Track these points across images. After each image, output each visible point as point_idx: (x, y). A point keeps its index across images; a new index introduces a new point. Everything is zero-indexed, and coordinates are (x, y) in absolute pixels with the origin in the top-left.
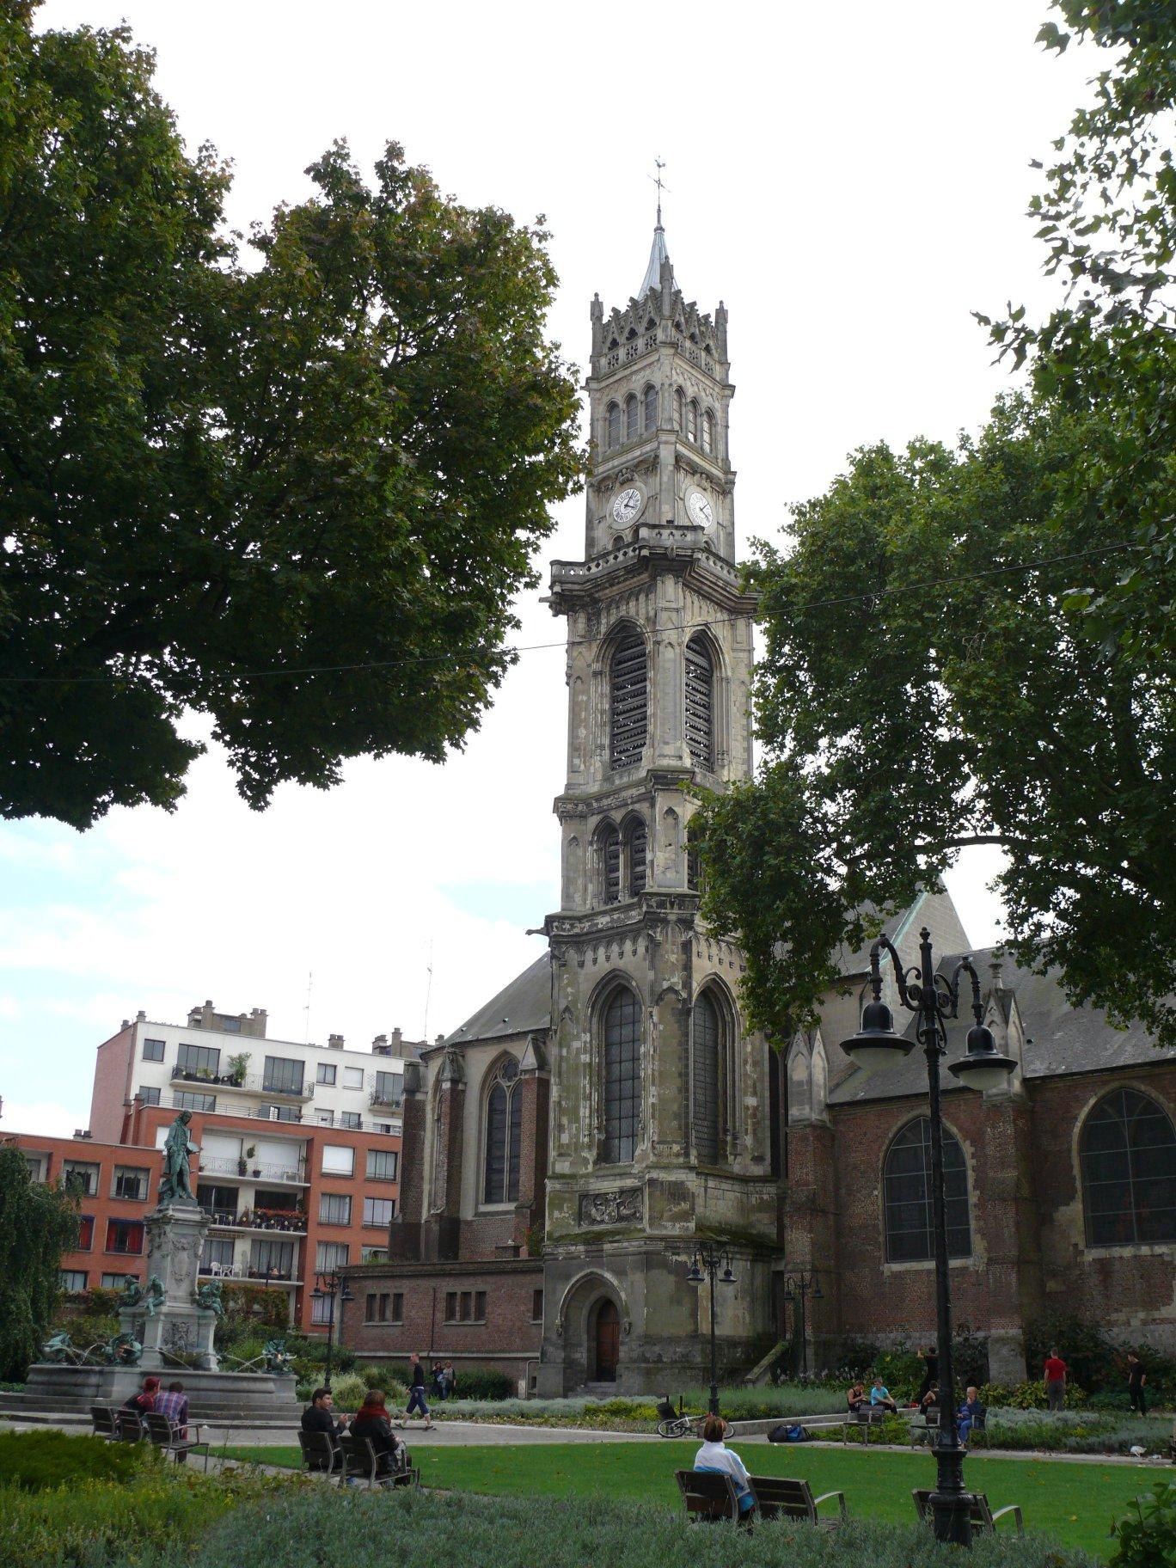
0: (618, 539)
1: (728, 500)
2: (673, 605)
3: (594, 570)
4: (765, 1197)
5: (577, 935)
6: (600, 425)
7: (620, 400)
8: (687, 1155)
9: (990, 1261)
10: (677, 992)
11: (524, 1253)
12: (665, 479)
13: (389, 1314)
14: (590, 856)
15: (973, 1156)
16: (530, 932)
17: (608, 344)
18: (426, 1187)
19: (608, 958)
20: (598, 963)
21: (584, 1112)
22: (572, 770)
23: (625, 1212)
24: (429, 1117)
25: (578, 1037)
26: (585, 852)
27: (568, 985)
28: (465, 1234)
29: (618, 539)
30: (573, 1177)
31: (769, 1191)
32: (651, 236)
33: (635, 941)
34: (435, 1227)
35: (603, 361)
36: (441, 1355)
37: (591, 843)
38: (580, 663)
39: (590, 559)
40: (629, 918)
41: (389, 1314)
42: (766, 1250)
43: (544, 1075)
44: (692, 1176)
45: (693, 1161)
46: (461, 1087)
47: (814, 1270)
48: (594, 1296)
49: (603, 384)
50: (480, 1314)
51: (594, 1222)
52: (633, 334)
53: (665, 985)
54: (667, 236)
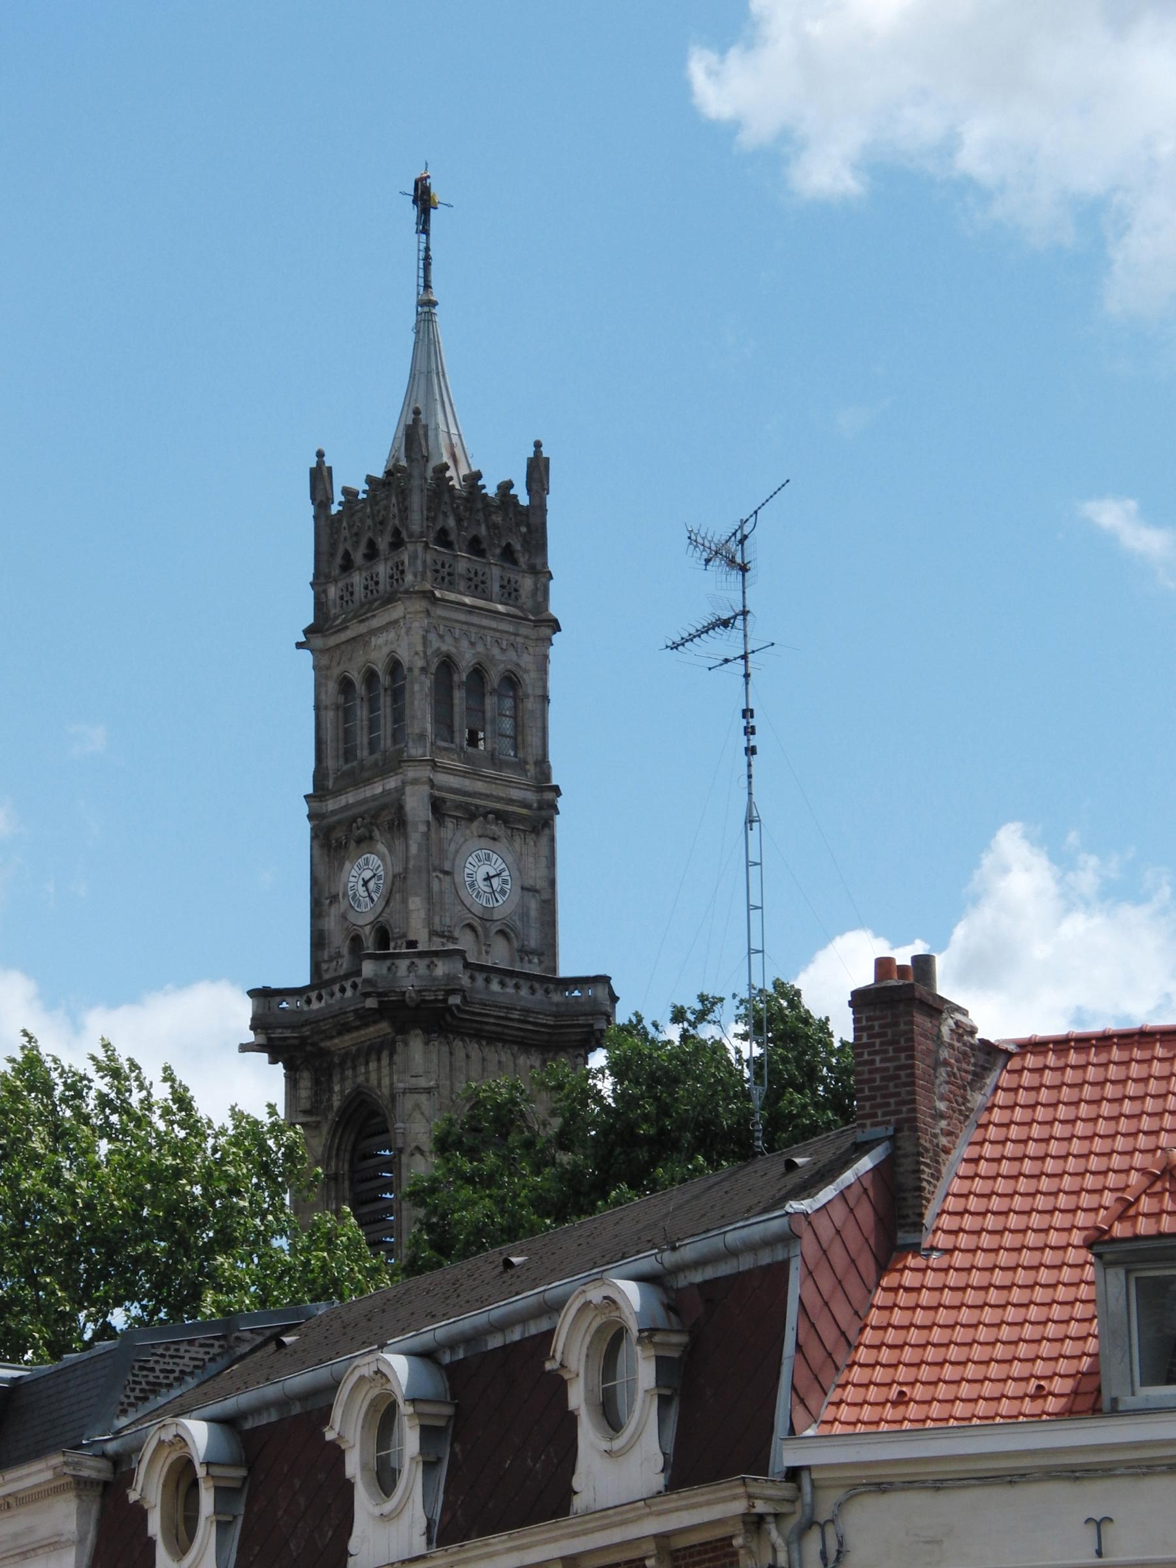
1: (544, 840)
2: (423, 1083)
6: (330, 715)
7: (356, 677)
12: (414, 849)
17: (339, 560)
29: (356, 941)
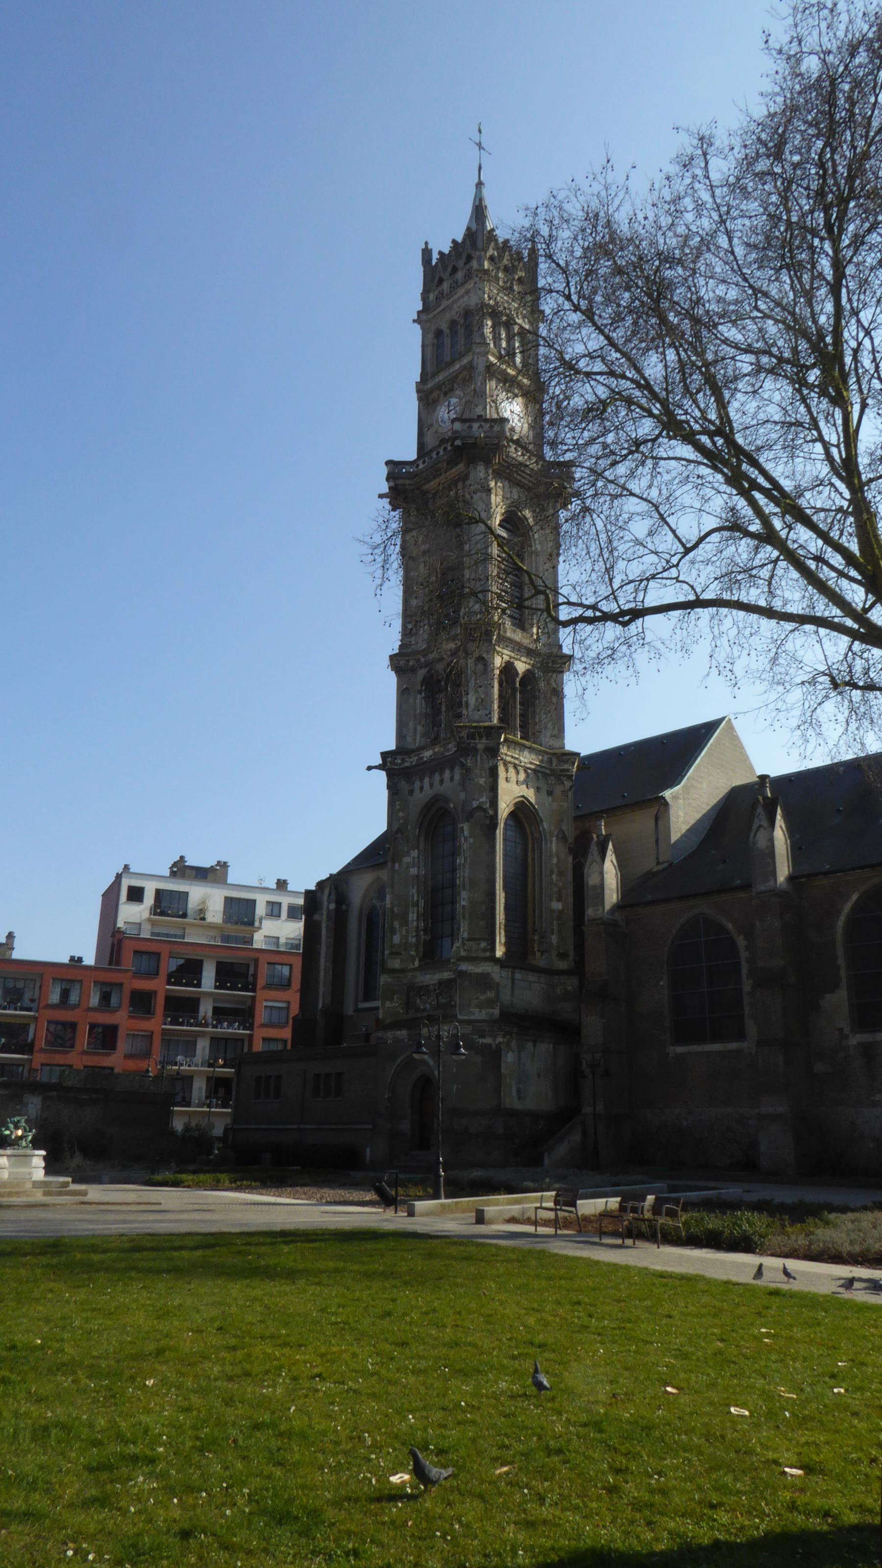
3: (421, 466)
4: (569, 988)
5: (407, 768)
6: (429, 350)
7: (444, 326)
10: (485, 810)
14: (419, 702)
15: (747, 948)
16: (369, 768)
19: (431, 785)
21: (412, 916)
23: (442, 1001)
25: (407, 854)
26: (415, 699)
27: (400, 810)
30: (402, 971)
31: (572, 983)
32: (473, 190)
33: (452, 770)
36: (308, 1126)
37: (420, 692)
40: (448, 750)
42: (566, 1032)
44: (497, 969)
46: (344, 907)
49: (431, 315)
52: (455, 270)
53: (475, 804)
54: (485, 192)
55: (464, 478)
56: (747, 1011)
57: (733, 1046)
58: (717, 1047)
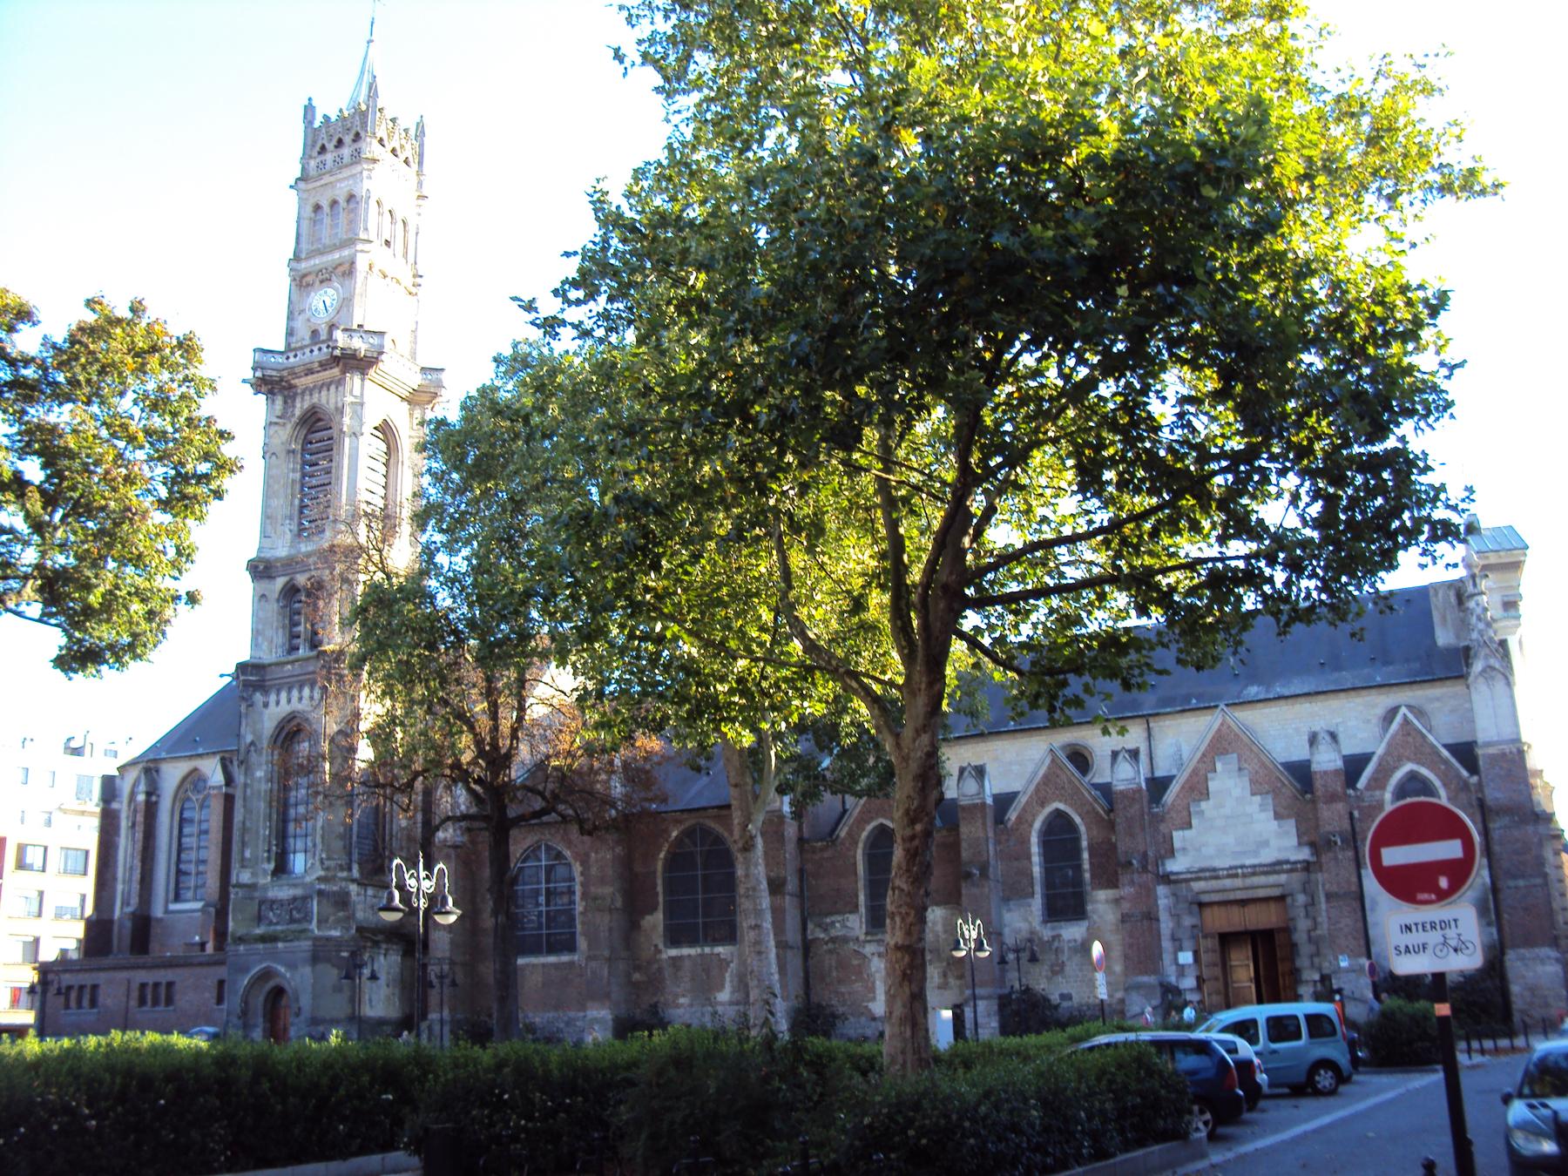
0: (315, 333)
3: (292, 360)
6: (305, 224)
7: (325, 204)
8: (350, 869)
9: (589, 958)
11: (210, 948)
13: (86, 1002)
16: (514, 299)
17: (318, 148)
18: (120, 887)
19: (289, 701)
20: (275, 709)
22: (264, 535)
24: (124, 824)
28: (156, 930)
29: (315, 333)
34: (129, 924)
35: (313, 163)
38: (276, 441)
39: (289, 348)
41: (86, 1002)
43: (230, 791)
45: (356, 873)
46: (154, 798)
47: (452, 963)
48: (271, 984)
49: (310, 186)
50: (169, 1001)
51: (271, 923)
52: (340, 143)
55: (340, 383)
56: (579, 927)
57: (565, 958)
58: (552, 959)
